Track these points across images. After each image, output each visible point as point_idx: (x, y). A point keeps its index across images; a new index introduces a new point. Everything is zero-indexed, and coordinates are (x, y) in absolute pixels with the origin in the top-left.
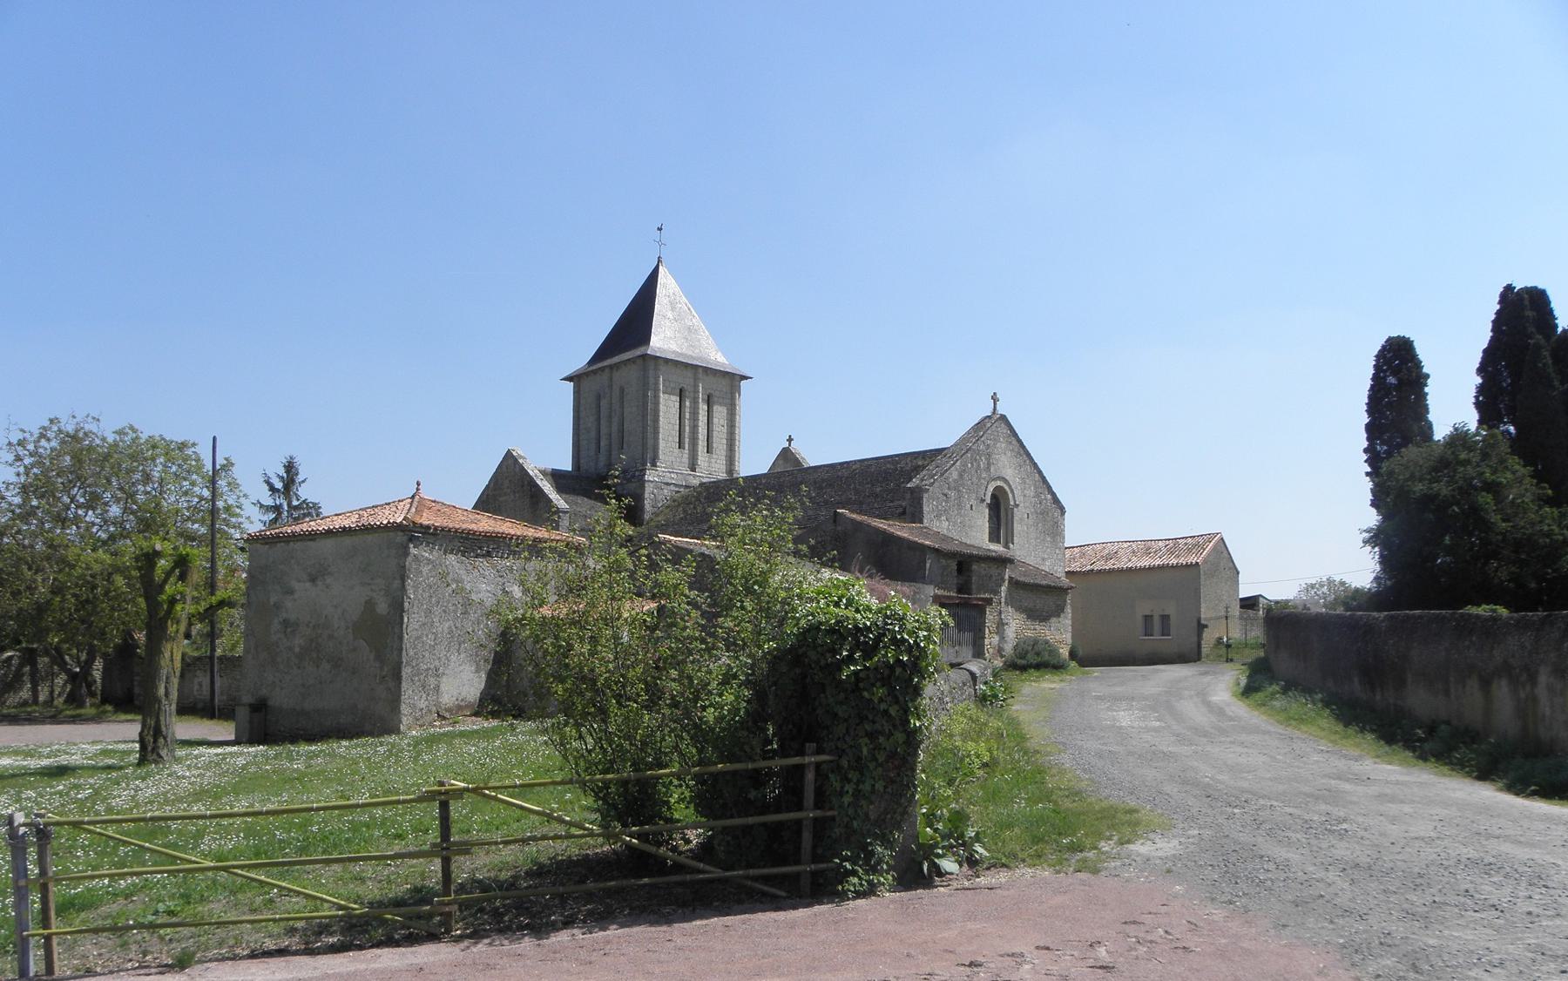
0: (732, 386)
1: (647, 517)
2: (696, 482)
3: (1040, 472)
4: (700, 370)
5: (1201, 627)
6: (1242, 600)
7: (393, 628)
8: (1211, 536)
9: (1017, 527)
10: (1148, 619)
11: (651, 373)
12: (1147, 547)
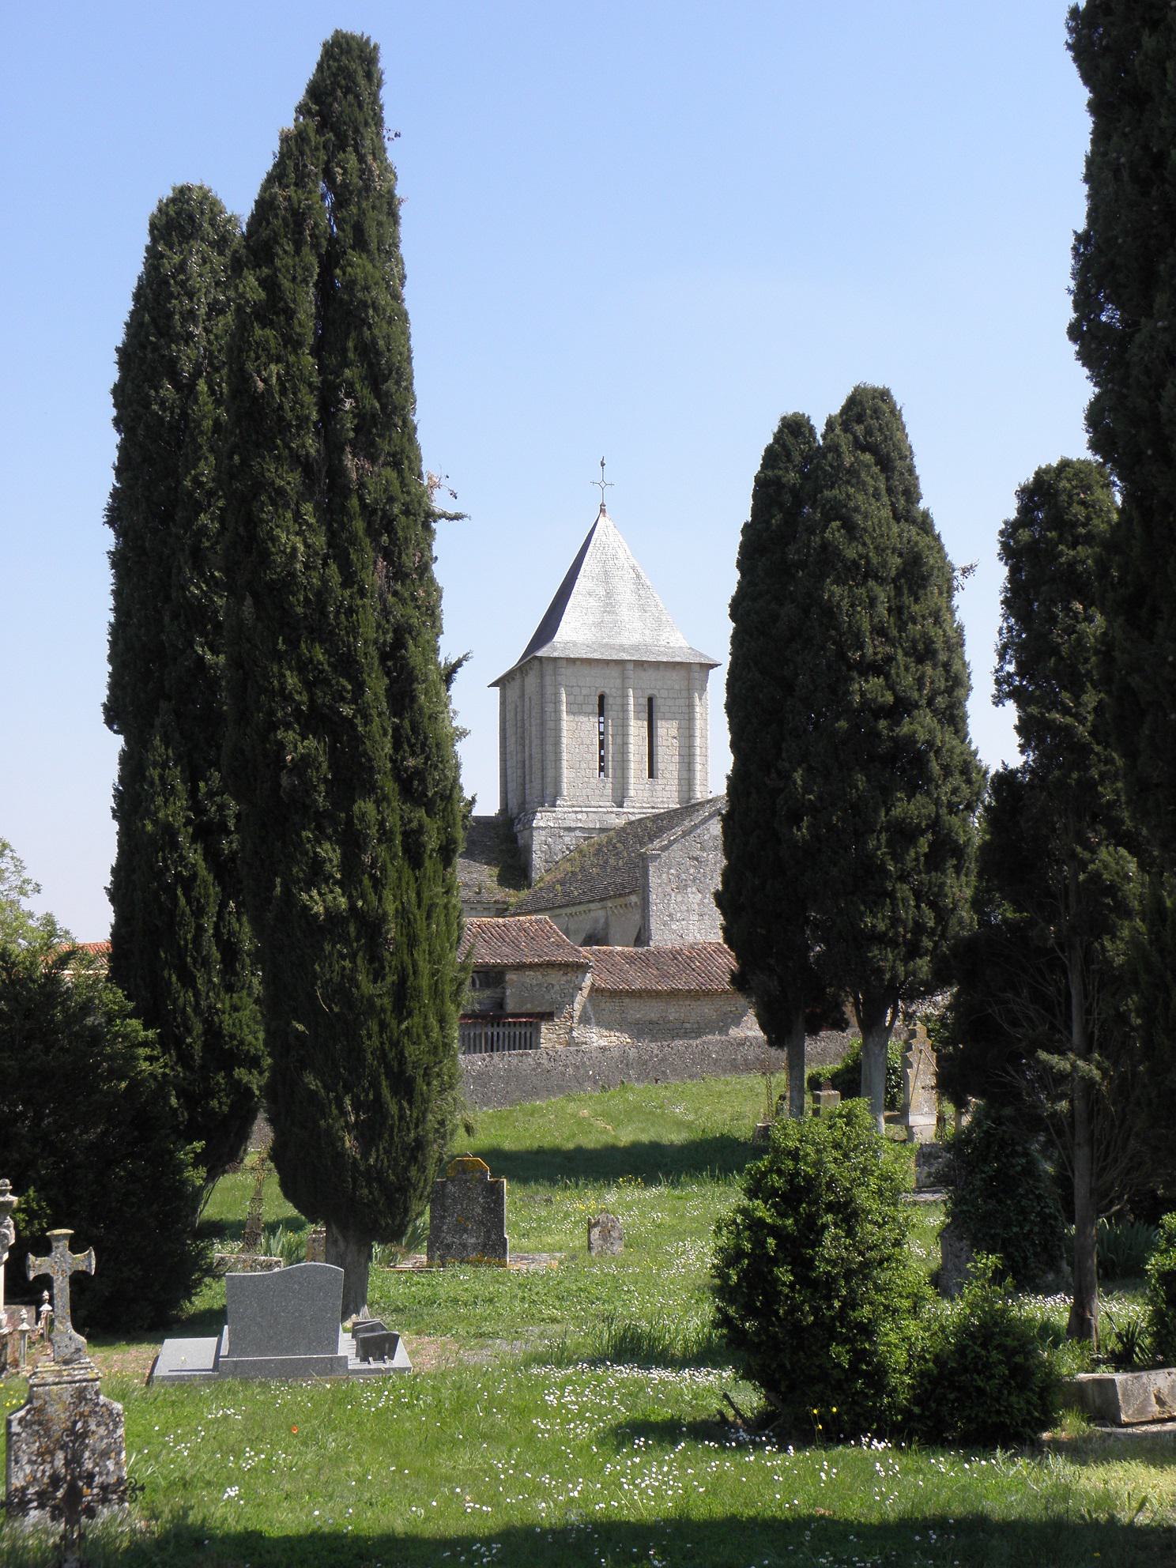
0: (689, 680)
1: (535, 876)
2: (620, 822)
4: (630, 666)
7: (544, 1411)
11: (548, 680)
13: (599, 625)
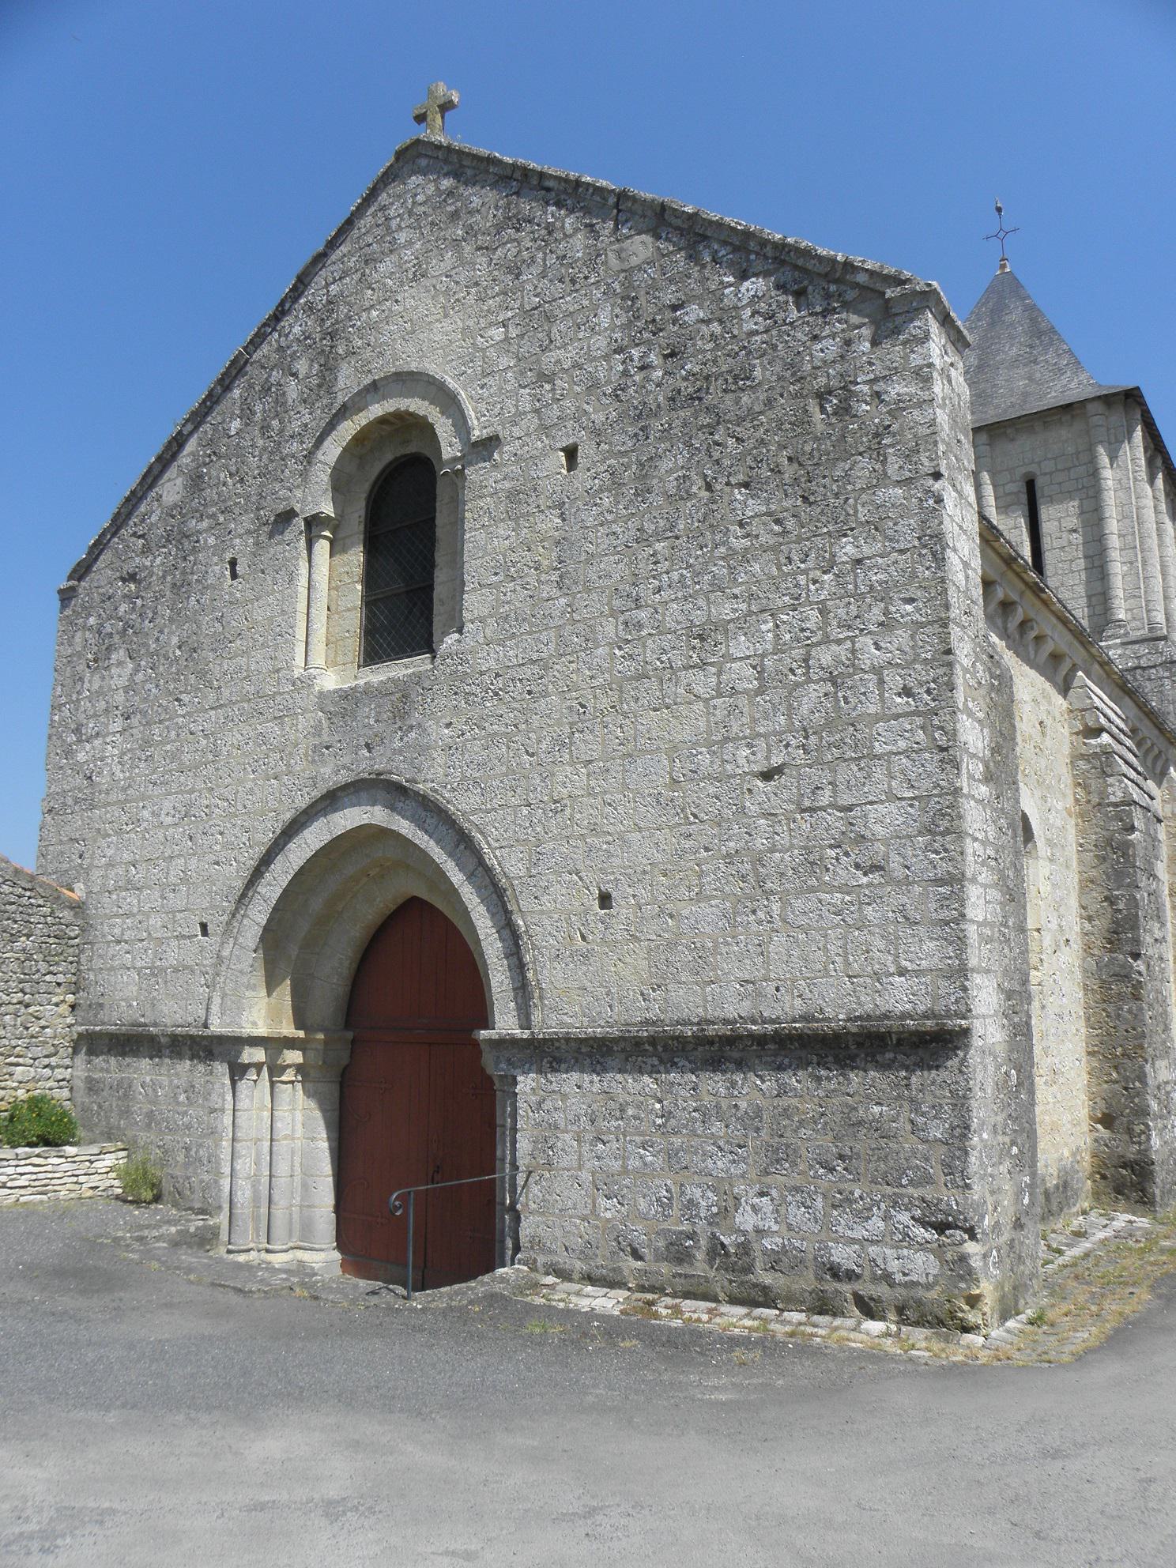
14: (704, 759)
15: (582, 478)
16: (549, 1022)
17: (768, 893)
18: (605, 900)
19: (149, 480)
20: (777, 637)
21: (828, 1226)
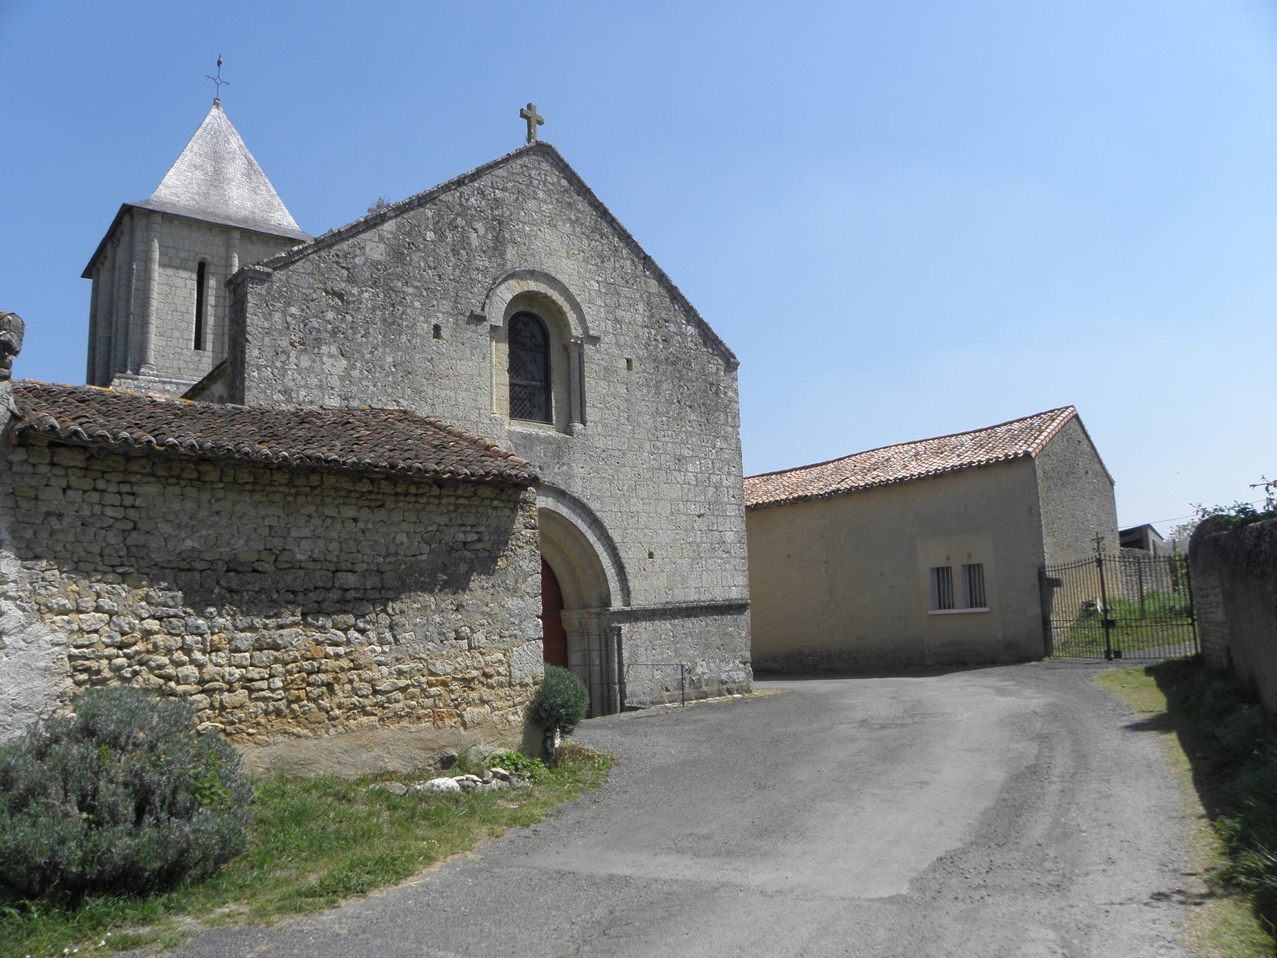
3: (661, 278)
4: (237, 235)
5: (1046, 585)
6: (1123, 534)
8: (1053, 414)
9: (595, 387)
10: (942, 574)
12: (941, 444)
13: (206, 195)
14: (681, 506)
15: (635, 377)
16: (640, 600)
17: (701, 558)
18: (651, 555)
19: (354, 231)
20: (701, 468)
21: (719, 667)
